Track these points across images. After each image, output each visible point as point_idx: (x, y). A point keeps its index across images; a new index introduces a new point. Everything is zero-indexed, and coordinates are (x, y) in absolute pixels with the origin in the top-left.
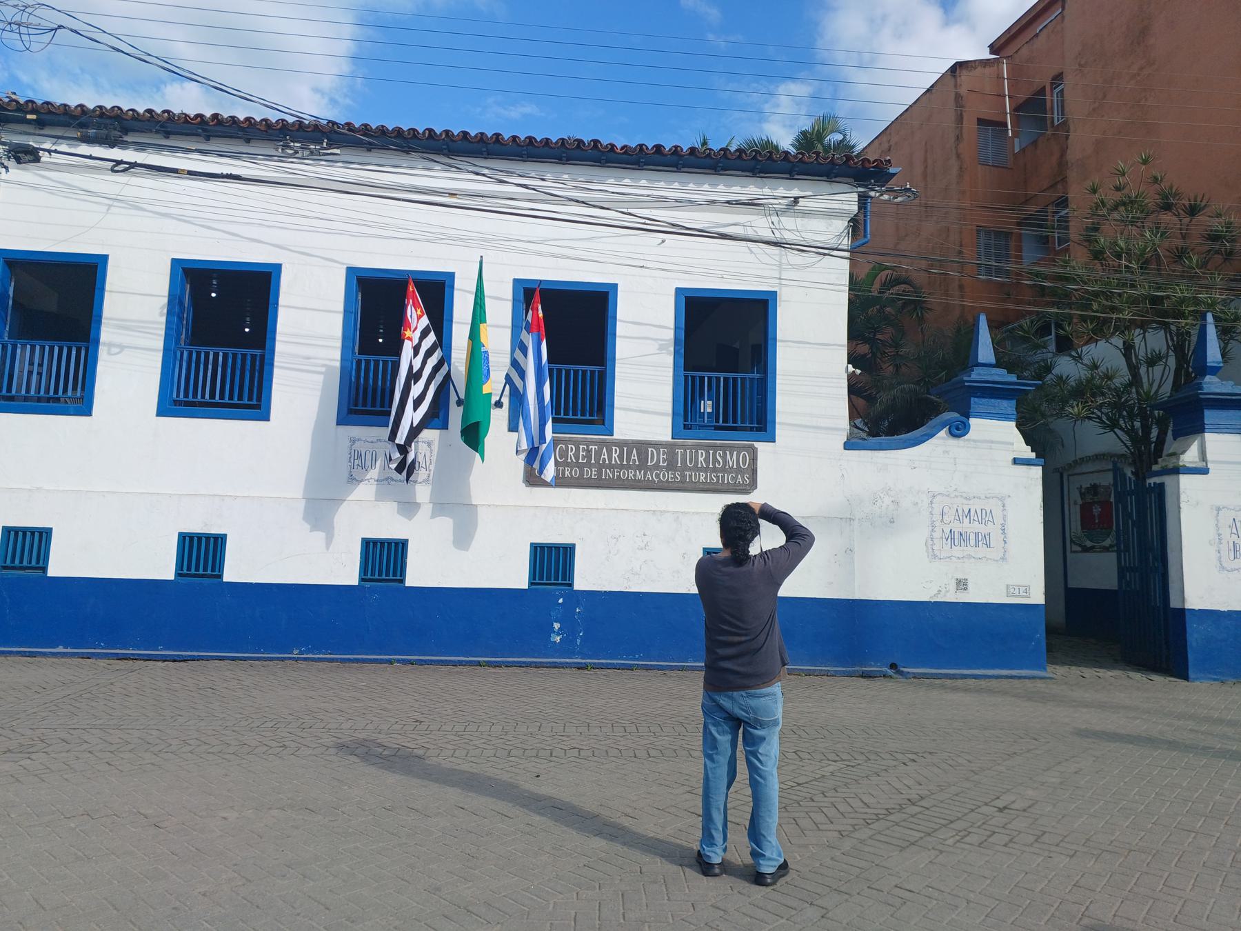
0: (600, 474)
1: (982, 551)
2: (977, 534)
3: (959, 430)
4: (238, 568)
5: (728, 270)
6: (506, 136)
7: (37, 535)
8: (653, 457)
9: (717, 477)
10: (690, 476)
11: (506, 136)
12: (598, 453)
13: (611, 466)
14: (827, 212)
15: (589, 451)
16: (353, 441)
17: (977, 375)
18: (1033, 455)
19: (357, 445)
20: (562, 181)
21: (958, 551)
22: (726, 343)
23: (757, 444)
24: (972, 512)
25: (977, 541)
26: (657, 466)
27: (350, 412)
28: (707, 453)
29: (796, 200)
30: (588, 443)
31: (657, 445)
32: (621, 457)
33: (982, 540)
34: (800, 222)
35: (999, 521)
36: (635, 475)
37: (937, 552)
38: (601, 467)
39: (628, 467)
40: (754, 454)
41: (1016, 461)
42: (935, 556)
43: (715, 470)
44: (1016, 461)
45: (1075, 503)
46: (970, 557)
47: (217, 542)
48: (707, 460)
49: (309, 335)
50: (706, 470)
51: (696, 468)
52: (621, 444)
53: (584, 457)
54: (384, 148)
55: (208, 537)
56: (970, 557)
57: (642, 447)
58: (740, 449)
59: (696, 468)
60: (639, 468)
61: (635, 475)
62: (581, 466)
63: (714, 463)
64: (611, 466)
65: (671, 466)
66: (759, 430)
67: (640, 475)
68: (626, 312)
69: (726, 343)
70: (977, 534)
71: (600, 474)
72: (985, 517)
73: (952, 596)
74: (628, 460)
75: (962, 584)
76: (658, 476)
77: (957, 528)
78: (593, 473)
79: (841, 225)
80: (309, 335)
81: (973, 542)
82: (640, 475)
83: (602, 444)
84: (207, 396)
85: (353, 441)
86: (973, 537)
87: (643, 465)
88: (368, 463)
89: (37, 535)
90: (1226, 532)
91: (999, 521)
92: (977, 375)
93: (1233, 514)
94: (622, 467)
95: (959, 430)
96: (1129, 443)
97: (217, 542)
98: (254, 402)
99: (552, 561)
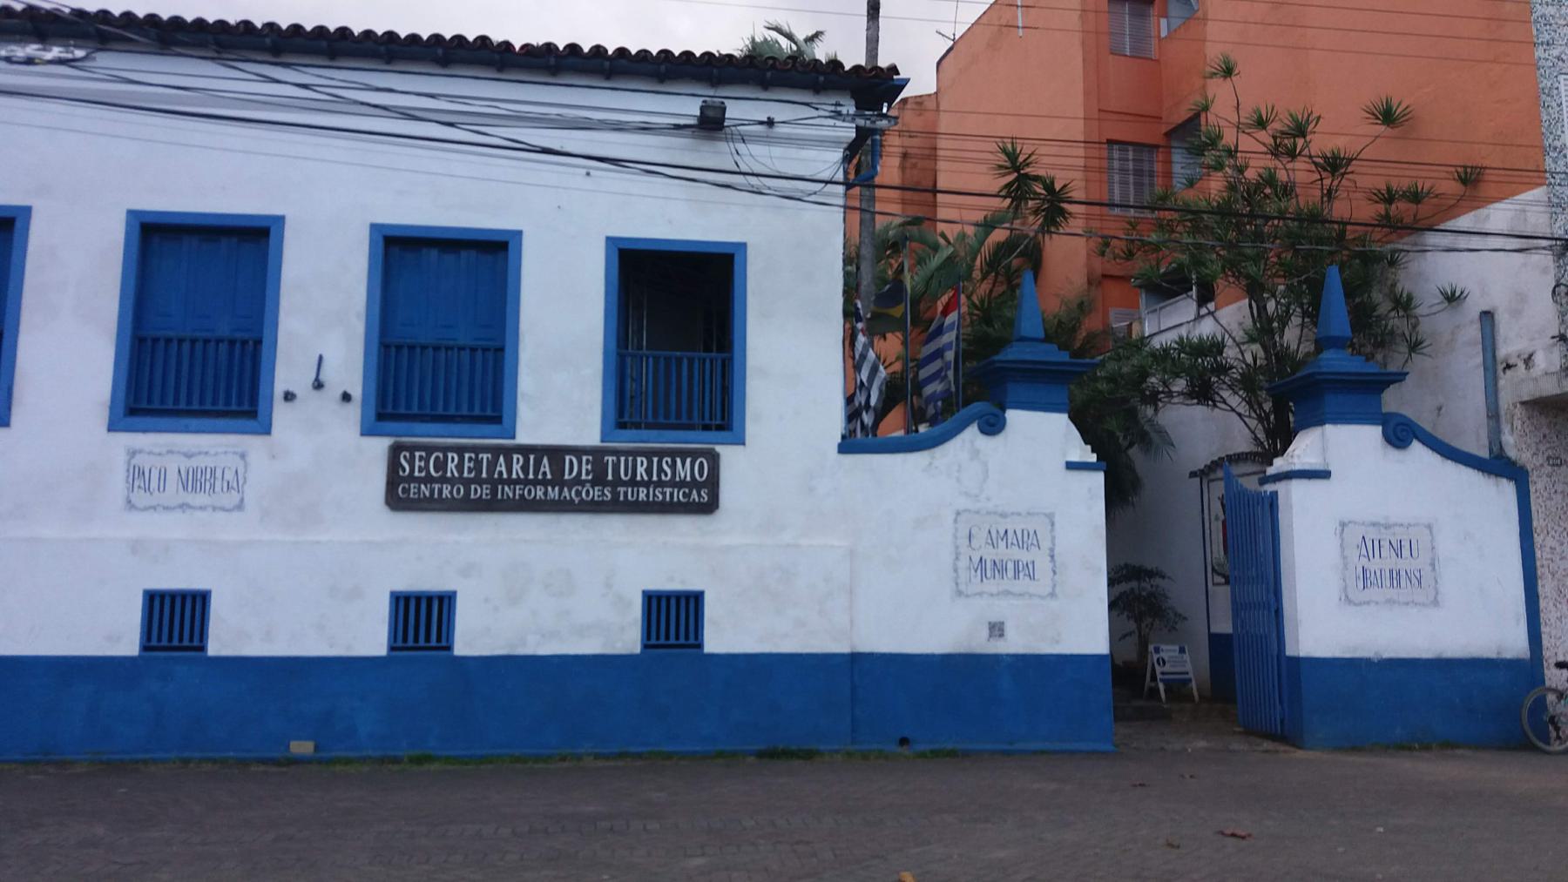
0: (494, 492)
1: (1023, 584)
2: (1016, 563)
3: (993, 426)
4: (231, 634)
5: (677, 216)
6: (357, 30)
7: (673, 602)
8: (572, 467)
9: (664, 494)
10: (626, 494)
11: (357, 30)
12: (492, 465)
13: (511, 482)
14: (814, 141)
15: (478, 463)
16: (133, 453)
17: (1012, 353)
18: (1093, 458)
19: (137, 461)
20: (286, 82)
21: (991, 585)
22: (677, 309)
23: (718, 448)
24: (1010, 533)
25: (1017, 572)
26: (578, 481)
27: (381, 417)
28: (650, 463)
29: (770, 123)
30: (477, 450)
31: (578, 451)
32: (525, 468)
33: (1023, 570)
34: (777, 151)
35: (1046, 544)
36: (546, 493)
37: (962, 587)
38: (494, 483)
39: (535, 482)
40: (714, 459)
41: (1071, 466)
42: (960, 593)
43: (660, 484)
44: (1071, 466)
45: (1217, 518)
46: (1007, 593)
47: (693, 601)
48: (649, 471)
49: (322, 320)
50: (647, 484)
51: (633, 483)
52: (526, 450)
53: (470, 471)
54: (202, 45)
55: (429, 598)
56: (1007, 593)
57: (556, 453)
58: (694, 454)
59: (633, 483)
60: (553, 483)
61: (546, 493)
62: (467, 483)
63: (659, 476)
64: (511, 482)
65: (599, 479)
66: (720, 428)
67: (553, 493)
68: (43, 247)
69: (677, 309)
70: (1016, 563)
71: (494, 492)
72: (1026, 540)
73: (982, 644)
74: (536, 472)
75: (997, 629)
76: (578, 493)
77: (989, 554)
78: (484, 492)
79: (837, 155)
80: (322, 320)
81: (1011, 573)
82: (553, 493)
83: (496, 451)
84: (209, 399)
85: (133, 453)
86: (1010, 566)
87: (558, 481)
88: (154, 484)
89: (673, 602)
90: (1353, 554)
91: (1046, 544)
92: (1012, 353)
93: (1361, 531)
94: (526, 482)
95: (993, 426)
96: (1262, 436)
97: (693, 601)
98: (246, 407)
99: (422, 616)
